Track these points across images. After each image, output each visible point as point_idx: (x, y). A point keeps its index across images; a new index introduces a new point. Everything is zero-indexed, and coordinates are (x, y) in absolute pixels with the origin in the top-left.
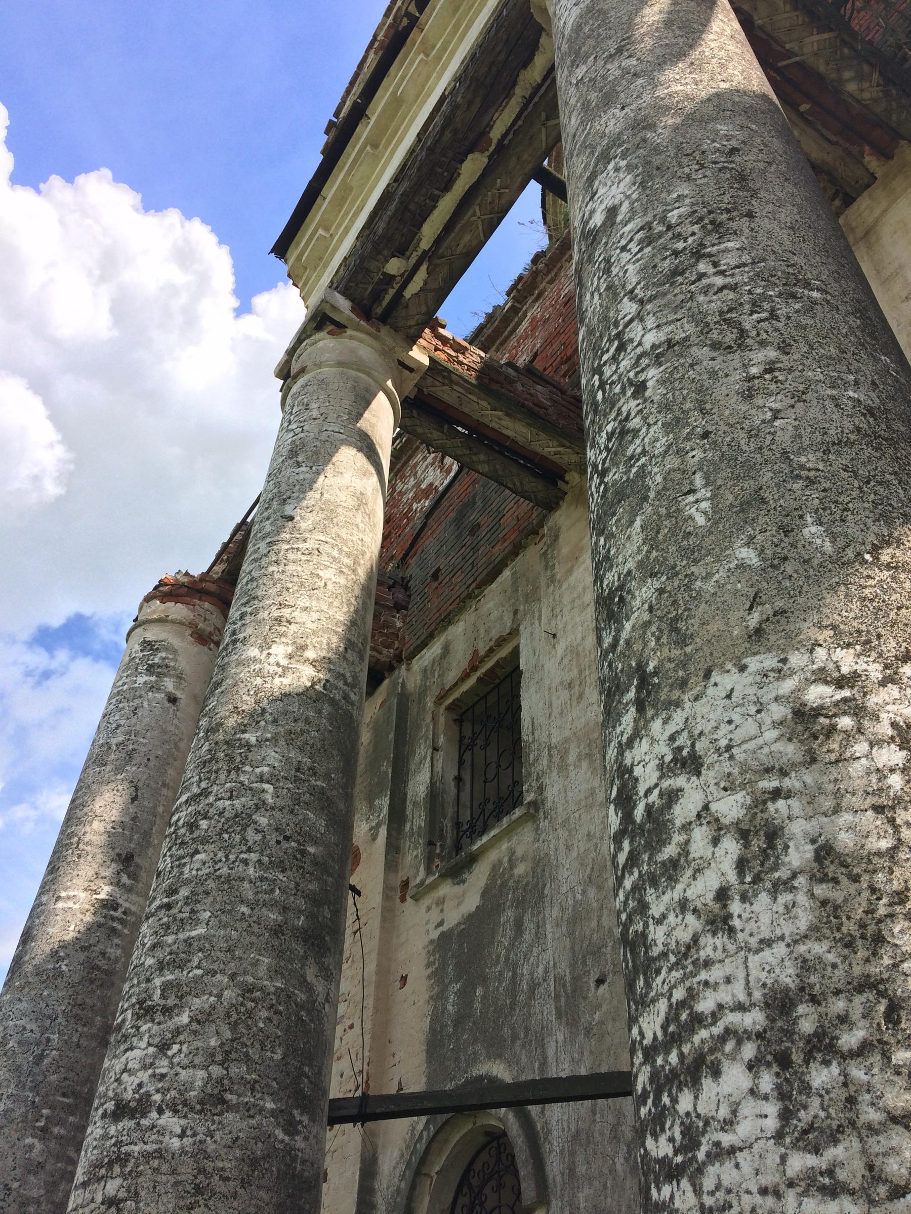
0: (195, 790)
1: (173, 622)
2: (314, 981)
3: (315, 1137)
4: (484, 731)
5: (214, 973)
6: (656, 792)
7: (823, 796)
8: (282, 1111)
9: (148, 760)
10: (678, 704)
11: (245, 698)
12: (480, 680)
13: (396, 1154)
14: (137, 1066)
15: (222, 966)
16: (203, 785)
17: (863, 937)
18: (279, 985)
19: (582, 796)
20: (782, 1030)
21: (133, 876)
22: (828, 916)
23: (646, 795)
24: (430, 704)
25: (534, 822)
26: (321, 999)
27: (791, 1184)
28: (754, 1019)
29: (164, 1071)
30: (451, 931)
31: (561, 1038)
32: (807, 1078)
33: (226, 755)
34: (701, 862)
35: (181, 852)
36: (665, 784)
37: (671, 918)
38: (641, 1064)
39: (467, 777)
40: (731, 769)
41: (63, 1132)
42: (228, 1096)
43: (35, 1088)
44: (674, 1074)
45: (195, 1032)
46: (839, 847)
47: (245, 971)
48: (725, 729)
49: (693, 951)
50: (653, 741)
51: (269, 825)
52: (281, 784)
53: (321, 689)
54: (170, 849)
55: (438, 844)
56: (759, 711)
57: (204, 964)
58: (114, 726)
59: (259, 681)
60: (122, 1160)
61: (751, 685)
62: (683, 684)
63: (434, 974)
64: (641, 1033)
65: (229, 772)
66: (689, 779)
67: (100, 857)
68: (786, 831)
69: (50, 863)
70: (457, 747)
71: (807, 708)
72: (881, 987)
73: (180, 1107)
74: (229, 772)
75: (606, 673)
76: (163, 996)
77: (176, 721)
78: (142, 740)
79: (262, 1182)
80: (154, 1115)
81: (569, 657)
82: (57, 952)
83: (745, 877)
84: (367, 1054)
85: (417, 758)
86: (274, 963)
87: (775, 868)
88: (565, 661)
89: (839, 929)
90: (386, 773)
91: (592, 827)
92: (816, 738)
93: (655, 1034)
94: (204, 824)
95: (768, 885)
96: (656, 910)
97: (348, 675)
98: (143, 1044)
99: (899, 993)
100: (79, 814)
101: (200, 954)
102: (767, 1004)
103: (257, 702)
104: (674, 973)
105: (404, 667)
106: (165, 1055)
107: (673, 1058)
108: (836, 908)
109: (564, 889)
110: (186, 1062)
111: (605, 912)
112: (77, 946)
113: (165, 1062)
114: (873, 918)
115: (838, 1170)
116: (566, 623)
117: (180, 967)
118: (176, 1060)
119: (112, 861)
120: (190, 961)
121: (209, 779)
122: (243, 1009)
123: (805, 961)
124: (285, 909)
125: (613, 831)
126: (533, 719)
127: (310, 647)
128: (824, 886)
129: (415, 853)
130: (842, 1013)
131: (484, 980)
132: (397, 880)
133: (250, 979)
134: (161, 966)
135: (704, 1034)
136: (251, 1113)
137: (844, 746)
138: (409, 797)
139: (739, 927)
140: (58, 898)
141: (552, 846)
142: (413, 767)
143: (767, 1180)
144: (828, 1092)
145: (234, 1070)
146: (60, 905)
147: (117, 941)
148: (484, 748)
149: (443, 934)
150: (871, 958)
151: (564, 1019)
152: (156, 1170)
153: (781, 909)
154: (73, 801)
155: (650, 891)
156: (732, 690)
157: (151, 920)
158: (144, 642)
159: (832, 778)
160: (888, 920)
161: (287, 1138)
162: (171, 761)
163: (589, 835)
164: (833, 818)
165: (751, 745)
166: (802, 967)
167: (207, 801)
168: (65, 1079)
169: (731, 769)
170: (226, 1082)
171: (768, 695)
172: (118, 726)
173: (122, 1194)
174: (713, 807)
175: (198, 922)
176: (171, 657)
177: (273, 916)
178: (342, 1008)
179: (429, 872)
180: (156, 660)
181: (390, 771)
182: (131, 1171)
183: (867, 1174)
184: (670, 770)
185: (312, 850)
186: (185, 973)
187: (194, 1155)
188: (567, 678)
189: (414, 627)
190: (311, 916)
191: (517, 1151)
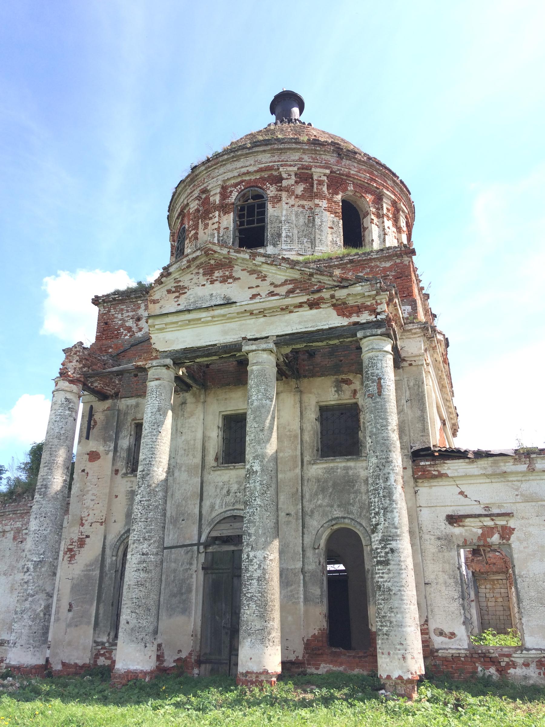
134: (147, 532)
140: (54, 478)
146: (55, 480)
172: (62, 428)
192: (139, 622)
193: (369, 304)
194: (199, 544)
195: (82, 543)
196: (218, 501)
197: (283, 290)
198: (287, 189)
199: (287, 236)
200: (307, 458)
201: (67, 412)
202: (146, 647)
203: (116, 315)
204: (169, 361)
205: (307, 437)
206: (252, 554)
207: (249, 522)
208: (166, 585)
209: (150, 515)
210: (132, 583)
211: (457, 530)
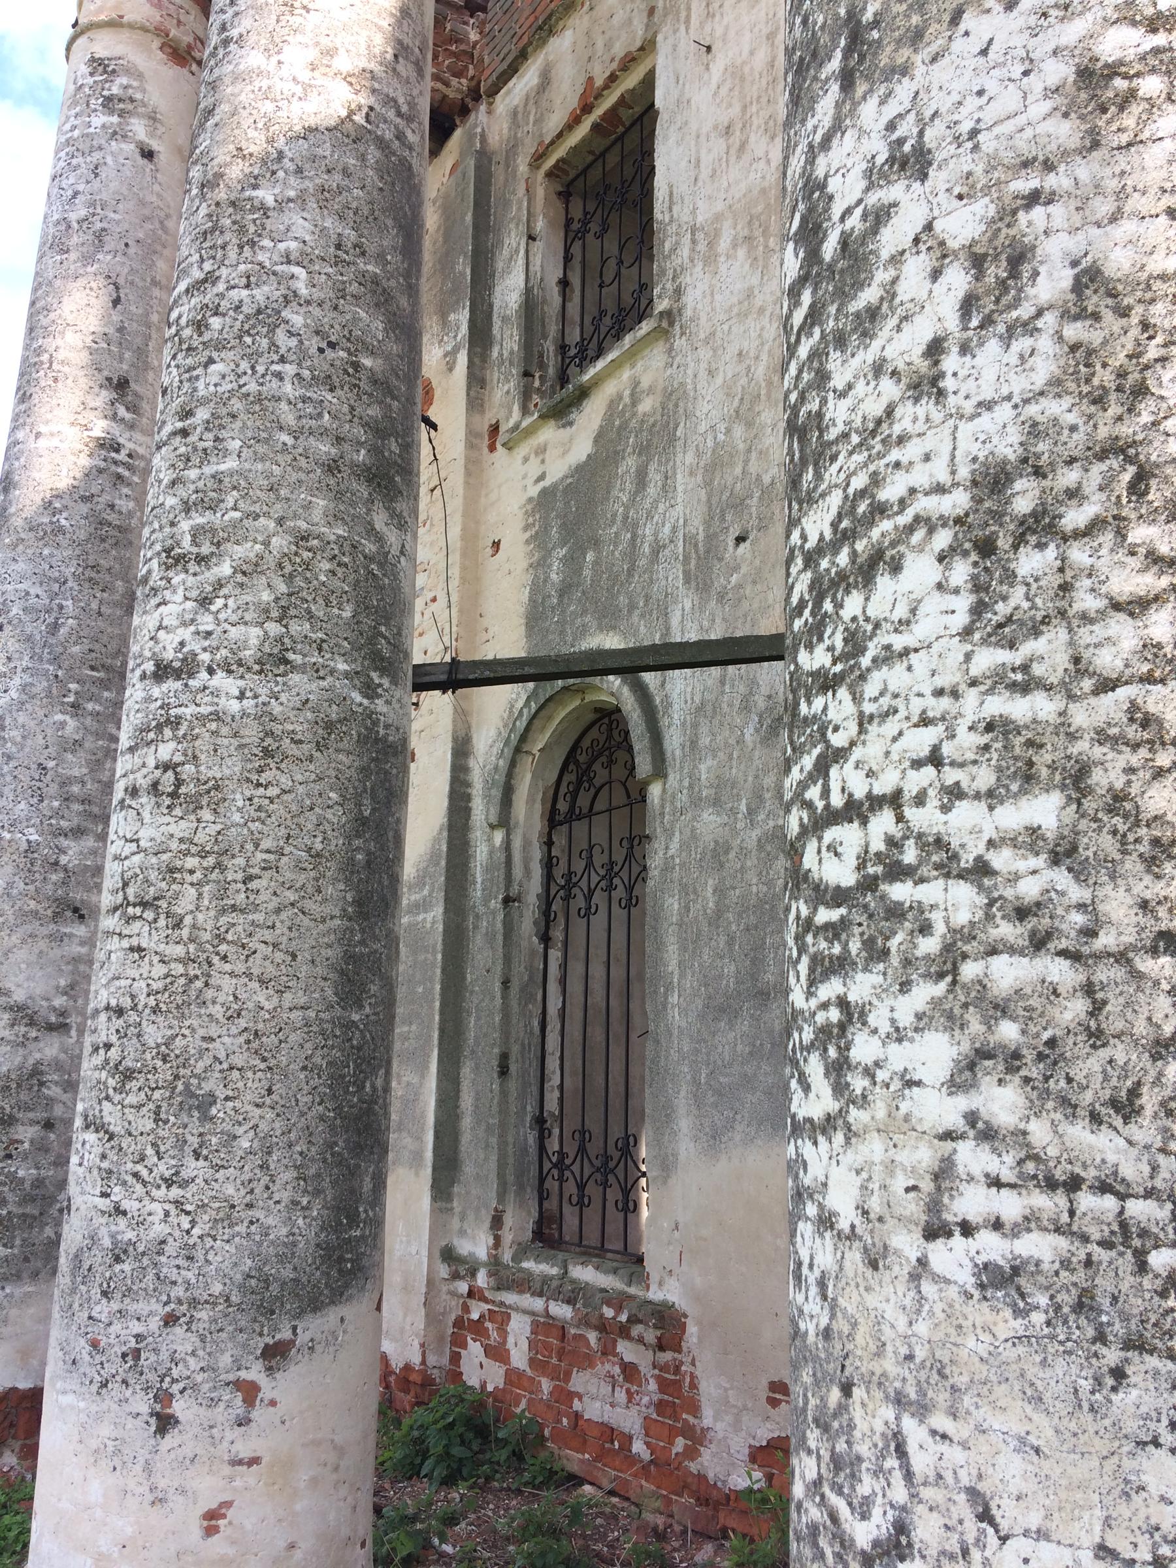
0: (197, 274)
1: (131, 26)
2: (385, 529)
3: (399, 701)
4: (599, 211)
5: (257, 517)
6: (858, 212)
7: (1100, 198)
8: (357, 673)
9: (127, 245)
10: (905, 70)
11: (252, 133)
12: (595, 127)
13: (493, 733)
14: (175, 623)
15: (265, 508)
16: (207, 266)
17: (1119, 389)
18: (340, 532)
19: (735, 300)
20: (990, 511)
21: (133, 408)
22: (1077, 364)
23: (842, 219)
24: (523, 168)
25: (667, 340)
26: (395, 551)
27: (973, 683)
28: (958, 501)
29: (209, 628)
30: (555, 486)
31: (688, 605)
32: (1012, 566)
33: (234, 223)
34: (908, 306)
35: (189, 361)
36: (872, 199)
37: (860, 388)
38: (800, 572)
39: (575, 280)
40: (972, 166)
41: (98, 708)
42: (291, 656)
43: (55, 660)
44: (842, 576)
45: (242, 585)
46: (1110, 270)
47: (295, 516)
48: (972, 102)
49: (884, 426)
50: (862, 133)
51: (306, 326)
52: (317, 268)
53: (363, 122)
54: (174, 357)
55: (537, 375)
56: (1026, 73)
57: (241, 504)
58: (70, 193)
59: (268, 107)
60: (175, 723)
61: (1021, 31)
62: (917, 37)
63: (534, 538)
64: (804, 537)
65: (241, 247)
66: (908, 187)
67: (84, 382)
68: (1039, 251)
69: (19, 389)
70: (562, 234)
71: (1099, 65)
72: (1132, 451)
73: (234, 667)
74: (241, 247)
75: (798, 35)
76: (194, 542)
77: (157, 188)
78: (112, 215)
79: (341, 745)
80: (204, 675)
81: (728, 85)
82: (50, 503)
83: (970, 320)
84: (454, 629)
85: (506, 252)
86: (332, 505)
87: (1016, 304)
88: (724, 91)
89: (1088, 381)
90: (463, 274)
91: (746, 344)
92: (1104, 110)
93: (821, 534)
94: (215, 322)
95: (1001, 328)
96: (838, 381)
97: (401, 100)
98: (179, 597)
99: (1153, 458)
100: (44, 322)
101: (235, 493)
102: (975, 483)
103: (271, 141)
104: (855, 457)
105: (483, 108)
106: (208, 610)
107: (843, 559)
108: (1090, 352)
109: (702, 428)
110: (234, 618)
111: (754, 455)
112: (76, 496)
113: (209, 618)
114: (1138, 364)
115: (1035, 665)
116: (727, 28)
117: (210, 508)
118: (222, 616)
119: (101, 386)
120: (223, 501)
121: (214, 258)
122: (298, 560)
123: (1035, 424)
124: (339, 440)
125: (789, 281)
126: (671, 187)
127: (342, 51)
128: (1079, 324)
129: (506, 388)
130: (1073, 486)
131: (596, 543)
132: (484, 427)
133: (303, 525)
134: (187, 508)
135: (886, 525)
136: (321, 673)
137: (1142, 122)
138: (495, 309)
139: (951, 389)
140: (38, 435)
141: (690, 372)
142: (500, 265)
143: (944, 680)
144: (1037, 580)
145: (295, 628)
146: (42, 443)
147: (125, 490)
148: (600, 236)
149: (544, 492)
150: (1126, 416)
151: (693, 584)
152: (215, 733)
153: (1014, 360)
154: (33, 303)
155: (835, 355)
156: (991, 41)
157: (164, 449)
158: (93, 60)
159: (1117, 170)
160: (1158, 366)
161: (365, 702)
162: (159, 248)
163: (740, 354)
164: (1108, 228)
165: (1008, 127)
166: (1029, 433)
167: (215, 290)
168: (91, 651)
169: (972, 166)
170: (286, 640)
171: (1042, 46)
172: (76, 194)
173: (178, 758)
174: (938, 226)
175: (226, 453)
176: (135, 84)
177: (325, 448)
178: (421, 580)
179: (525, 411)
180: (115, 90)
181: (468, 271)
182: (185, 735)
183: (1071, 667)
184: (883, 175)
185: (367, 362)
186: (219, 515)
187: (257, 718)
188: (724, 120)
189: (496, 41)
190: (375, 451)
191: (631, 726)
192: (119, 1211)
201: (99, 120)
202: (165, 1423)
208: (683, 949)
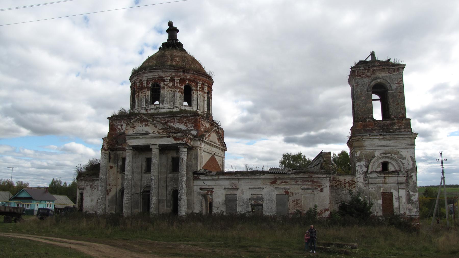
193: (181, 138)
194: (141, 193)
195: (110, 190)
196: (145, 182)
197: (161, 131)
198: (167, 85)
199: (166, 102)
200: (168, 172)
203: (115, 124)
204: (131, 148)
205: (168, 166)
206: (152, 198)
207: (152, 191)
209: (128, 188)
210: (125, 203)
211: (202, 191)
